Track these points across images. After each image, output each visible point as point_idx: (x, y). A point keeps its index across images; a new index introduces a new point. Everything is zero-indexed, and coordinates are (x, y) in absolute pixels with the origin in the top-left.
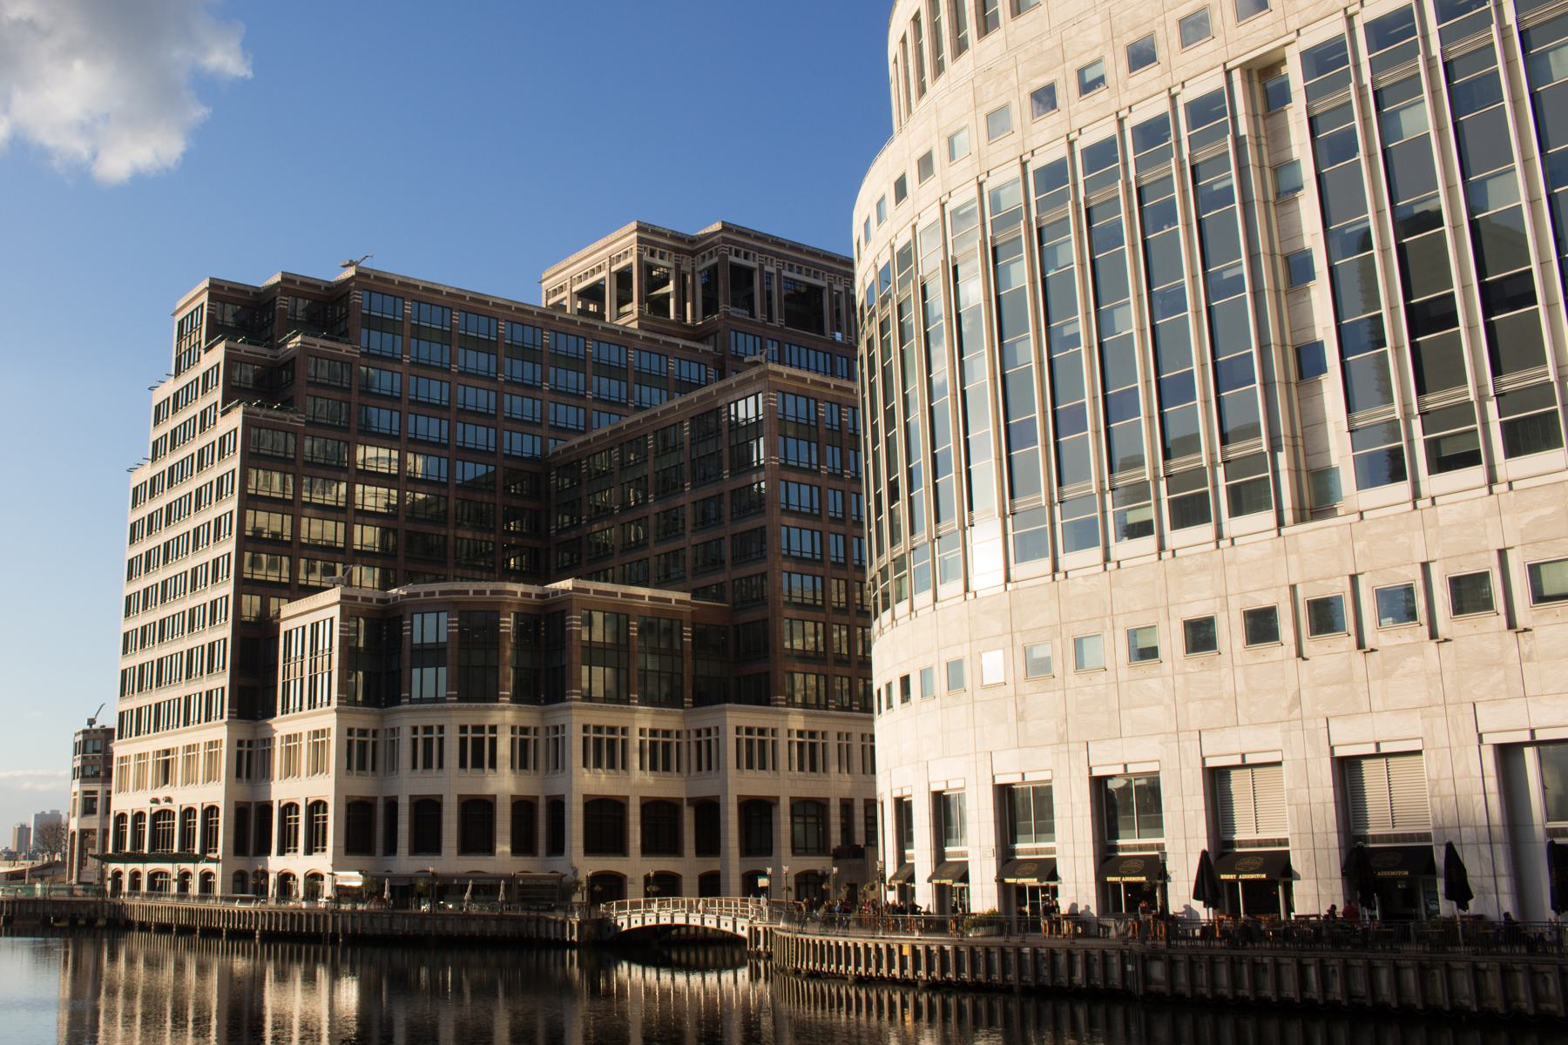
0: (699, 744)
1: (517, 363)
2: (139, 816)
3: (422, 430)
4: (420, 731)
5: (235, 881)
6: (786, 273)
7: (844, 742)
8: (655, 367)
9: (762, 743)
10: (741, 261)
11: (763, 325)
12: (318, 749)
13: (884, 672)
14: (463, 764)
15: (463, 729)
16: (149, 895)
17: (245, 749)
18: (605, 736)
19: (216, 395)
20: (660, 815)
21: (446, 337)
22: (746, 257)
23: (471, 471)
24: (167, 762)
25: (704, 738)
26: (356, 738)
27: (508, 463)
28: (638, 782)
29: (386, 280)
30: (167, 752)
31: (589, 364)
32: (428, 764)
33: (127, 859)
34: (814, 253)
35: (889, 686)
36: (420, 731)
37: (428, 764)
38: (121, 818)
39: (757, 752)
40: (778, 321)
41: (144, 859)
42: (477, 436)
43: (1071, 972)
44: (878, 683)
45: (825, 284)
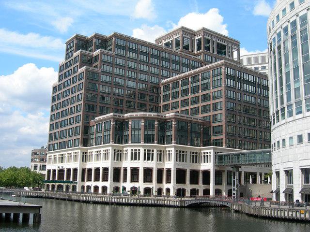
0: (118, 154)
1: (142, 56)
2: (54, 171)
3: (130, 74)
4: (116, 151)
5: (81, 188)
6: (217, 41)
7: (85, 154)
8: (177, 59)
9: (196, 156)
10: (207, 37)
11: (212, 53)
12: (76, 156)
13: (274, 141)
14: (145, 160)
15: (132, 150)
16: (51, 191)
17: (85, 154)
18: (206, 154)
19: (78, 64)
20: (148, 172)
21: (168, 60)
22: (224, 42)
23: (142, 86)
24: (62, 157)
25: (120, 152)
26: (178, 152)
27: (152, 85)
28: (141, 164)
29: (134, 39)
30: (62, 155)
31: (256, 84)
32: (118, 160)
33: (52, 182)
34: (212, 32)
35: (275, 144)
36: (116, 151)
37: (148, 159)
38: (49, 171)
39: (135, 156)
40: (215, 53)
41: (56, 182)
42: (143, 77)
43: (266, 213)
44: (272, 143)
45: (210, 38)
